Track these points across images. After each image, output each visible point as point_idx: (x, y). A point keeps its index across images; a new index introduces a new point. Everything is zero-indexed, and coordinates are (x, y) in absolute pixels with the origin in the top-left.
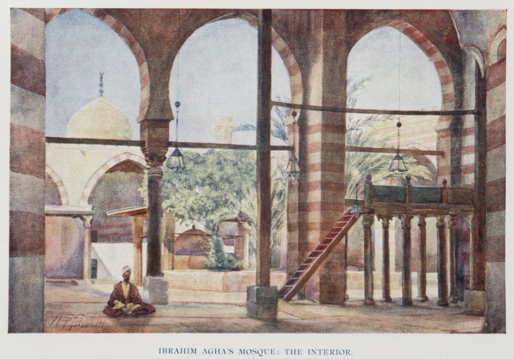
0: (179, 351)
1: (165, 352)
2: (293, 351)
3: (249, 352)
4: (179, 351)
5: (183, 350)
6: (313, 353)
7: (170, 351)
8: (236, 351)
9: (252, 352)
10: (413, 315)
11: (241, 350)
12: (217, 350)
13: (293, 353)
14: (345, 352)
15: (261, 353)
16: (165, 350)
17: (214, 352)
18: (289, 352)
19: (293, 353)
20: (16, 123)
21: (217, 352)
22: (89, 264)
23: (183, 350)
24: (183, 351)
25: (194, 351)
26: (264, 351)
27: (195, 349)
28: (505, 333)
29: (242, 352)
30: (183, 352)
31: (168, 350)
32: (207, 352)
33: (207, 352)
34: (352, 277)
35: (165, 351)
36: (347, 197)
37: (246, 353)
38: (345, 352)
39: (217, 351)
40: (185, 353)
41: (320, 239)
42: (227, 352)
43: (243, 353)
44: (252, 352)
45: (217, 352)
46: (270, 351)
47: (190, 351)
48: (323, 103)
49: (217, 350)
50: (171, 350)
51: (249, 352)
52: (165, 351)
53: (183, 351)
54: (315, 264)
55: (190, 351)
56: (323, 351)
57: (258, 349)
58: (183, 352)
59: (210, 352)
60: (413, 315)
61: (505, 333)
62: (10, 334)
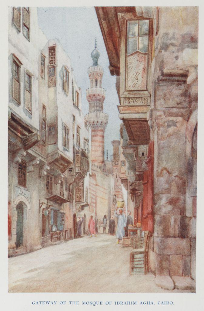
0: (127, 303)
1: (118, 304)
2: (74, 302)
3: (88, 303)
4: (127, 303)
5: (129, 302)
7: (122, 303)
8: (138, 303)
9: (92, 303)
11: (49, 304)
12: (148, 302)
13: (74, 303)
14: (86, 303)
15: (94, 304)
16: (118, 302)
17: (147, 303)
18: (72, 303)
19: (74, 303)
21: (148, 304)
22: (57, 76)
23: (129, 302)
24: (129, 303)
26: (96, 303)
28: (195, 293)
29: (84, 303)
30: (129, 304)
31: (120, 303)
32: (143, 303)
33: (143, 303)
35: (118, 303)
37: (109, 303)
38: (63, 303)
41: (120, 125)
44: (92, 303)
45: (148, 304)
46: (150, 304)
47: (133, 303)
49: (148, 302)
50: (122, 302)
51: (88, 303)
52: (118, 303)
53: (129, 303)
54: (61, 197)
55: (133, 303)
57: (92, 301)
58: (129, 304)
59: (144, 303)
61: (195, 293)
62: (196, 291)
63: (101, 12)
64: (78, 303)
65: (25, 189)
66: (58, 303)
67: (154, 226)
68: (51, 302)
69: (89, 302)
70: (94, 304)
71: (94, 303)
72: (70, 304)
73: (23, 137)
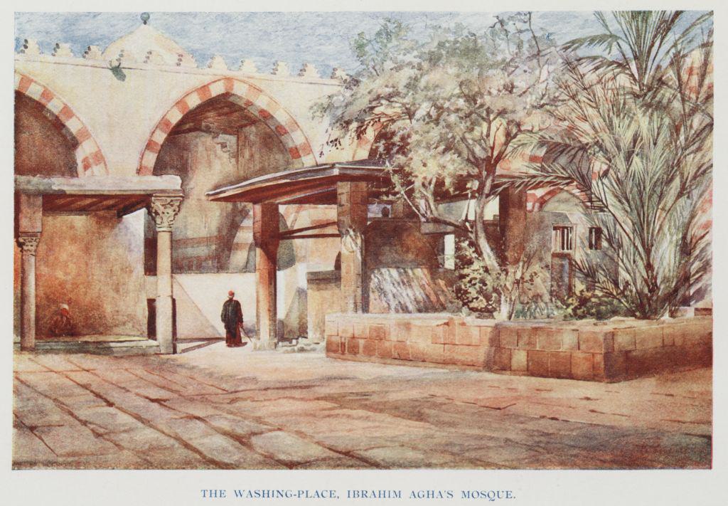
1: (356, 496)
2: (213, 492)
3: (475, 495)
5: (382, 492)
6: (279, 495)
7: (364, 495)
10: (287, 397)
13: (213, 495)
14: (470, 495)
15: (266, 494)
17: (426, 496)
18: (208, 494)
19: (213, 495)
20: (21, 367)
21: (431, 496)
23: (382, 492)
24: (382, 494)
25: (398, 495)
26: (496, 495)
27: (433, 492)
29: (466, 495)
31: (360, 494)
32: (417, 496)
33: (417, 496)
34: (361, 350)
35: (356, 494)
36: (497, 174)
39: (430, 494)
40: (433, 497)
42: (445, 495)
43: (467, 496)
46: (505, 493)
48: (165, 133)
50: (364, 492)
51: (475, 495)
52: (356, 494)
53: (382, 494)
55: (276, 493)
56: (209, 491)
57: (487, 489)
58: (382, 496)
59: (421, 496)
60: (287, 397)
63: (75, 174)
64: (332, 496)
65: (397, 413)
66: (406, 494)
67: (68, 193)
68: (247, 492)
69: (480, 492)
70: (266, 494)
71: (491, 495)
72: (349, 491)
73: (653, 431)
